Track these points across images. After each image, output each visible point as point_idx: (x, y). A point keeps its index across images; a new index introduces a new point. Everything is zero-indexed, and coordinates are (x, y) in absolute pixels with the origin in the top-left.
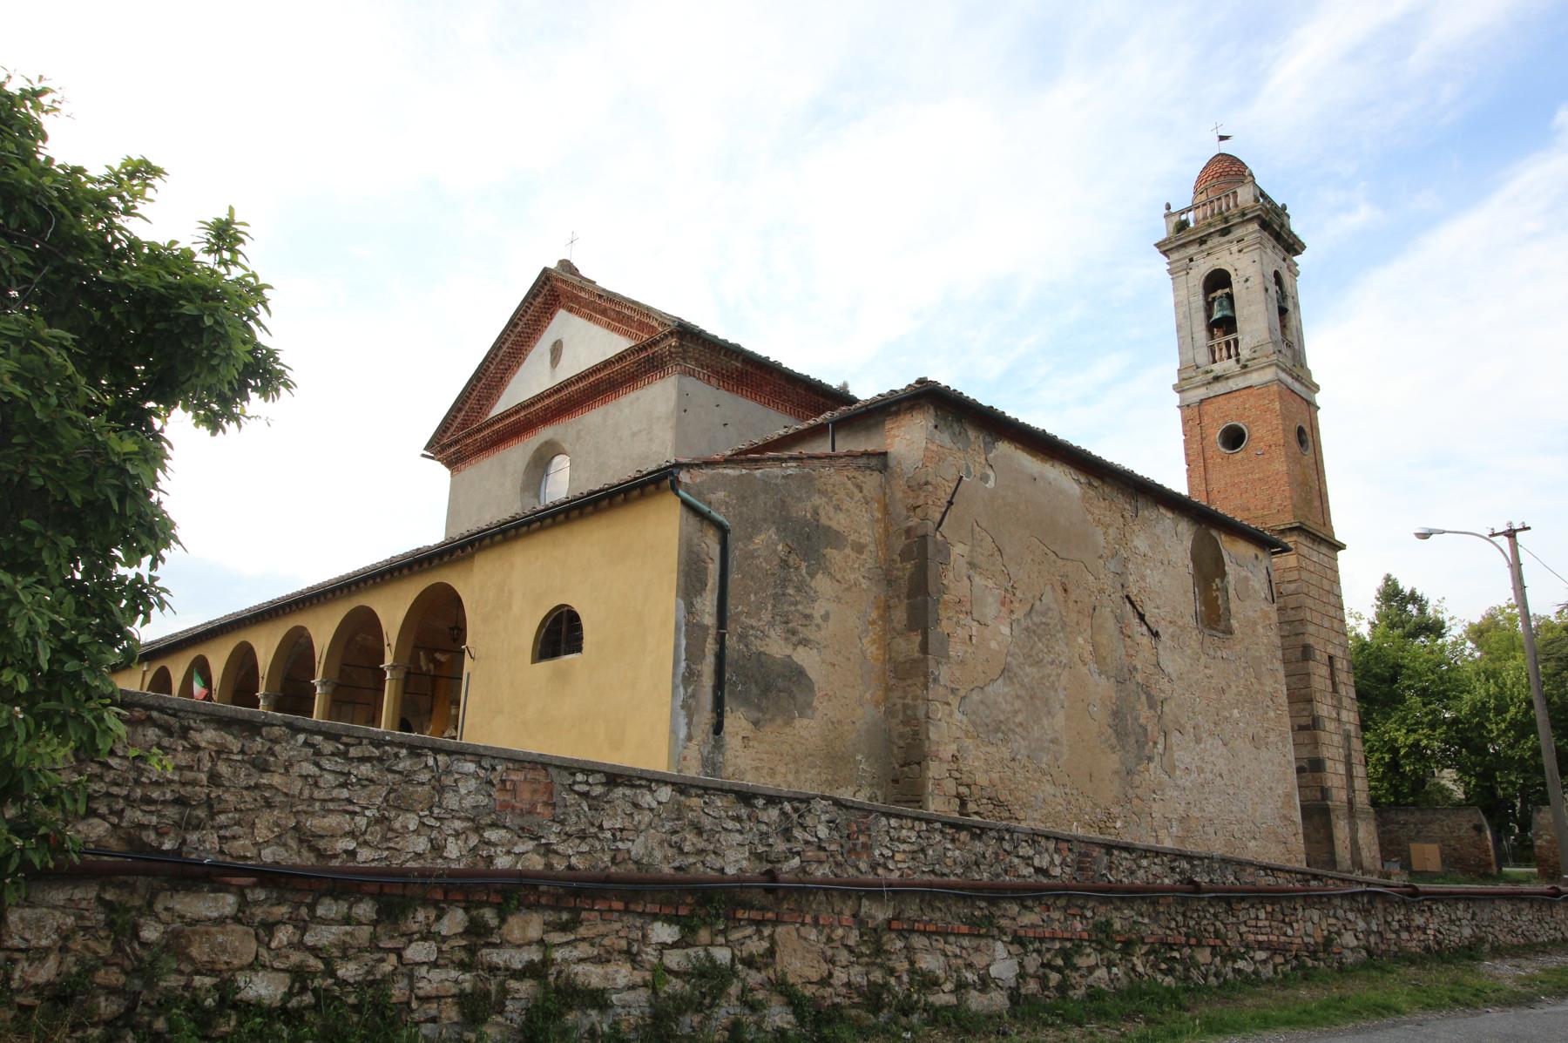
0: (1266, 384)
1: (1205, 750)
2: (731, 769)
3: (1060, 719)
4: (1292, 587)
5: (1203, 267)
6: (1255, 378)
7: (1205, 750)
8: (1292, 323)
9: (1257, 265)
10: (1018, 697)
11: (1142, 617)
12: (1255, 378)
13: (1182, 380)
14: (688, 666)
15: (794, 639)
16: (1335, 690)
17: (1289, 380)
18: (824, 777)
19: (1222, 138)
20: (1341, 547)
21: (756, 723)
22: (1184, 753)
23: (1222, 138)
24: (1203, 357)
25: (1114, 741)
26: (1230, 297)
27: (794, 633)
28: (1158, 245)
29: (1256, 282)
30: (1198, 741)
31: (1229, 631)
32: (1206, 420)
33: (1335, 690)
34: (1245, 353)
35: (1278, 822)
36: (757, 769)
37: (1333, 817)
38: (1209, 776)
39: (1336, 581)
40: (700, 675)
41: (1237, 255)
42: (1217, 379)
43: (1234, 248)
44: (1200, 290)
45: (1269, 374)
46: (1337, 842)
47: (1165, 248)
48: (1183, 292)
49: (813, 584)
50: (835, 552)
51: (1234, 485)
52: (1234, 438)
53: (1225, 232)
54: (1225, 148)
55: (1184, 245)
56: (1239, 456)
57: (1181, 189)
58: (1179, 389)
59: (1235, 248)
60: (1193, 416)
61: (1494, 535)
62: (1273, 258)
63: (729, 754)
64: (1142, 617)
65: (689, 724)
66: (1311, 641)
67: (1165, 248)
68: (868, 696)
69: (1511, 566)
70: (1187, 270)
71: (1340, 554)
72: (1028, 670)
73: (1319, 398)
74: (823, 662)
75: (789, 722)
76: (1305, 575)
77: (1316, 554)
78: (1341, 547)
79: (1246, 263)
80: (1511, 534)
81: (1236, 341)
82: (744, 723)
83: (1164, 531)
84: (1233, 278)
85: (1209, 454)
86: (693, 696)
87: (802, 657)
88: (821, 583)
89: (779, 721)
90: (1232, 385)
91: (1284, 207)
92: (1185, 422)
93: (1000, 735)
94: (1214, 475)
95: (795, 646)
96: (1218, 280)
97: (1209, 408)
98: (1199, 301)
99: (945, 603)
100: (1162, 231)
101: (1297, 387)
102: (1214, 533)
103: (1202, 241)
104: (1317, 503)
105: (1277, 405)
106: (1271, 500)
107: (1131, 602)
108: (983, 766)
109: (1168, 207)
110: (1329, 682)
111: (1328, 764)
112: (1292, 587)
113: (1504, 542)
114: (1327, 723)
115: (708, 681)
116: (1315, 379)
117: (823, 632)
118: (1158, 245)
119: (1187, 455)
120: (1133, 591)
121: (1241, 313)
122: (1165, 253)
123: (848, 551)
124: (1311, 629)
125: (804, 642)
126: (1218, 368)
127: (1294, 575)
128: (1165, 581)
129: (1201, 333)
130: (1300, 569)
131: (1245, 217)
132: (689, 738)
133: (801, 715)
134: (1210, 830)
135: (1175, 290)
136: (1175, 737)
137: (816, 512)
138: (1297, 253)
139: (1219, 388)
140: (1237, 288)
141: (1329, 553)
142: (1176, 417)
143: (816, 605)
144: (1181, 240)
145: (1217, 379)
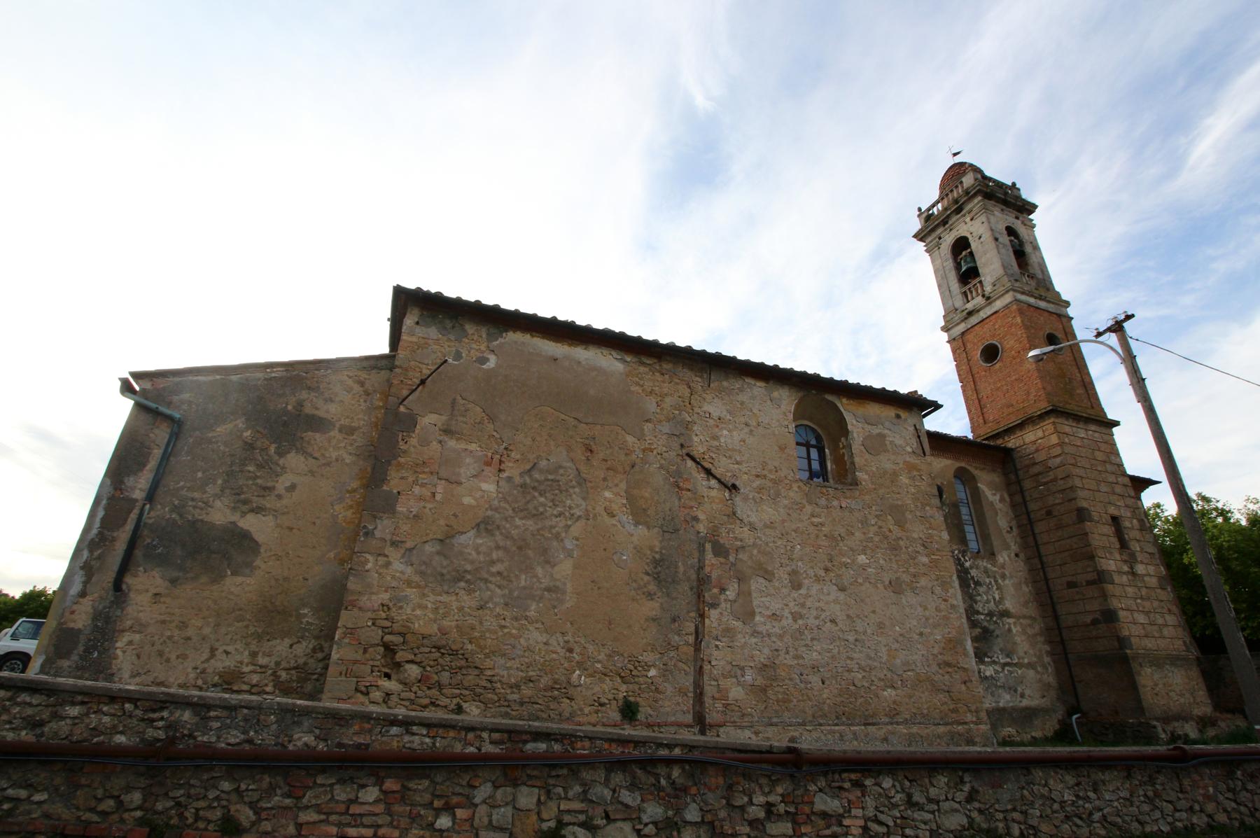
0: (1006, 307)
1: (808, 596)
2: (129, 623)
3: (565, 568)
4: (1058, 460)
5: (949, 239)
6: (998, 305)
7: (808, 596)
8: (1033, 259)
9: (986, 224)
10: (498, 547)
11: (708, 472)
12: (998, 305)
13: (946, 322)
14: (100, 533)
15: (245, 508)
16: (1123, 545)
17: (1032, 300)
18: (252, 629)
19: (955, 155)
20: (1116, 424)
21: (174, 582)
22: (769, 599)
23: (955, 155)
24: (959, 302)
25: (652, 587)
26: (971, 254)
27: (245, 502)
28: (915, 236)
29: (987, 236)
30: (796, 586)
31: (855, 483)
32: (969, 346)
33: (1123, 545)
34: (988, 289)
35: (935, 668)
36: (163, 622)
37: (1135, 666)
38: (812, 622)
39: (1118, 455)
40: (114, 540)
41: (970, 223)
42: (970, 314)
43: (977, 223)
44: (949, 256)
45: (1008, 298)
46: (1142, 690)
47: (920, 236)
48: (938, 262)
49: (281, 462)
50: (317, 435)
51: (998, 389)
52: (991, 353)
53: (959, 210)
54: (958, 159)
55: (933, 230)
56: (997, 366)
57: (928, 194)
58: (945, 329)
59: (968, 219)
60: (959, 345)
61: (1099, 334)
62: (1002, 219)
63: (131, 610)
64: (708, 472)
65: (85, 583)
66: (1084, 504)
67: (920, 236)
68: (332, 555)
69: (1124, 361)
70: (938, 246)
71: (1115, 430)
72: (518, 522)
73: (1071, 311)
74: (278, 526)
75: (218, 578)
76: (1068, 449)
77: (1093, 432)
78: (1116, 424)
79: (977, 227)
80: (1117, 327)
81: (981, 282)
82: (159, 581)
83: (753, 398)
84: (970, 239)
85: (975, 370)
86: (99, 558)
87: (250, 523)
88: (293, 460)
89: (204, 579)
90: (982, 315)
91: (1014, 184)
92: (954, 352)
93: (462, 584)
94: (981, 386)
95: (244, 514)
96: (961, 245)
97: (969, 337)
98: (950, 264)
99: (399, 464)
100: (917, 225)
101: (1042, 304)
102: (830, 397)
103: (944, 222)
104: (1080, 391)
105: (1019, 320)
106: (1028, 394)
107: (693, 459)
108: (423, 613)
109: (920, 209)
110: (1114, 540)
111: (1122, 614)
112: (1058, 460)
113: (1112, 339)
114: (1116, 578)
115: (120, 547)
116: (1064, 297)
117: (284, 502)
118: (915, 236)
119: (959, 375)
120: (699, 450)
121: (981, 262)
122: (921, 240)
123: (335, 433)
124: (1081, 494)
125: (258, 510)
126: (970, 306)
127: (1058, 451)
128: (750, 440)
129: (955, 285)
130: (1061, 444)
131: (969, 195)
132: (83, 594)
133: (234, 573)
134: (815, 680)
135: (933, 262)
136: (757, 584)
137: (300, 404)
138: (1031, 212)
139: (974, 320)
140: (974, 246)
141: (1103, 430)
142: (947, 350)
143: (281, 479)
144: (930, 227)
145: (970, 314)
